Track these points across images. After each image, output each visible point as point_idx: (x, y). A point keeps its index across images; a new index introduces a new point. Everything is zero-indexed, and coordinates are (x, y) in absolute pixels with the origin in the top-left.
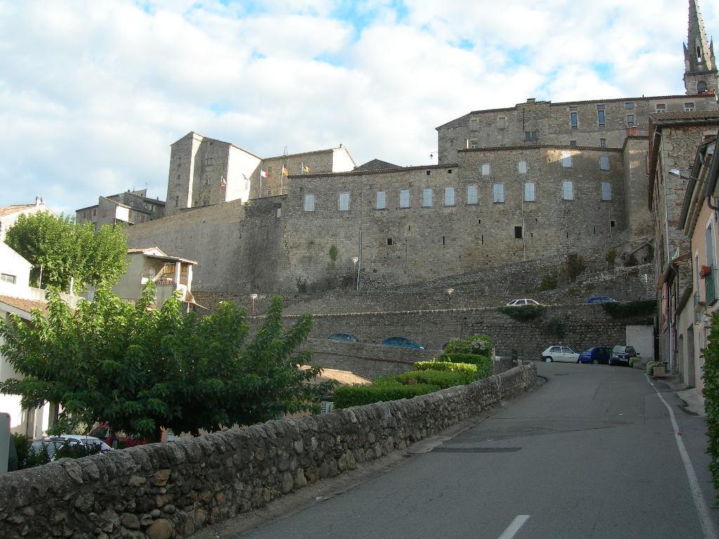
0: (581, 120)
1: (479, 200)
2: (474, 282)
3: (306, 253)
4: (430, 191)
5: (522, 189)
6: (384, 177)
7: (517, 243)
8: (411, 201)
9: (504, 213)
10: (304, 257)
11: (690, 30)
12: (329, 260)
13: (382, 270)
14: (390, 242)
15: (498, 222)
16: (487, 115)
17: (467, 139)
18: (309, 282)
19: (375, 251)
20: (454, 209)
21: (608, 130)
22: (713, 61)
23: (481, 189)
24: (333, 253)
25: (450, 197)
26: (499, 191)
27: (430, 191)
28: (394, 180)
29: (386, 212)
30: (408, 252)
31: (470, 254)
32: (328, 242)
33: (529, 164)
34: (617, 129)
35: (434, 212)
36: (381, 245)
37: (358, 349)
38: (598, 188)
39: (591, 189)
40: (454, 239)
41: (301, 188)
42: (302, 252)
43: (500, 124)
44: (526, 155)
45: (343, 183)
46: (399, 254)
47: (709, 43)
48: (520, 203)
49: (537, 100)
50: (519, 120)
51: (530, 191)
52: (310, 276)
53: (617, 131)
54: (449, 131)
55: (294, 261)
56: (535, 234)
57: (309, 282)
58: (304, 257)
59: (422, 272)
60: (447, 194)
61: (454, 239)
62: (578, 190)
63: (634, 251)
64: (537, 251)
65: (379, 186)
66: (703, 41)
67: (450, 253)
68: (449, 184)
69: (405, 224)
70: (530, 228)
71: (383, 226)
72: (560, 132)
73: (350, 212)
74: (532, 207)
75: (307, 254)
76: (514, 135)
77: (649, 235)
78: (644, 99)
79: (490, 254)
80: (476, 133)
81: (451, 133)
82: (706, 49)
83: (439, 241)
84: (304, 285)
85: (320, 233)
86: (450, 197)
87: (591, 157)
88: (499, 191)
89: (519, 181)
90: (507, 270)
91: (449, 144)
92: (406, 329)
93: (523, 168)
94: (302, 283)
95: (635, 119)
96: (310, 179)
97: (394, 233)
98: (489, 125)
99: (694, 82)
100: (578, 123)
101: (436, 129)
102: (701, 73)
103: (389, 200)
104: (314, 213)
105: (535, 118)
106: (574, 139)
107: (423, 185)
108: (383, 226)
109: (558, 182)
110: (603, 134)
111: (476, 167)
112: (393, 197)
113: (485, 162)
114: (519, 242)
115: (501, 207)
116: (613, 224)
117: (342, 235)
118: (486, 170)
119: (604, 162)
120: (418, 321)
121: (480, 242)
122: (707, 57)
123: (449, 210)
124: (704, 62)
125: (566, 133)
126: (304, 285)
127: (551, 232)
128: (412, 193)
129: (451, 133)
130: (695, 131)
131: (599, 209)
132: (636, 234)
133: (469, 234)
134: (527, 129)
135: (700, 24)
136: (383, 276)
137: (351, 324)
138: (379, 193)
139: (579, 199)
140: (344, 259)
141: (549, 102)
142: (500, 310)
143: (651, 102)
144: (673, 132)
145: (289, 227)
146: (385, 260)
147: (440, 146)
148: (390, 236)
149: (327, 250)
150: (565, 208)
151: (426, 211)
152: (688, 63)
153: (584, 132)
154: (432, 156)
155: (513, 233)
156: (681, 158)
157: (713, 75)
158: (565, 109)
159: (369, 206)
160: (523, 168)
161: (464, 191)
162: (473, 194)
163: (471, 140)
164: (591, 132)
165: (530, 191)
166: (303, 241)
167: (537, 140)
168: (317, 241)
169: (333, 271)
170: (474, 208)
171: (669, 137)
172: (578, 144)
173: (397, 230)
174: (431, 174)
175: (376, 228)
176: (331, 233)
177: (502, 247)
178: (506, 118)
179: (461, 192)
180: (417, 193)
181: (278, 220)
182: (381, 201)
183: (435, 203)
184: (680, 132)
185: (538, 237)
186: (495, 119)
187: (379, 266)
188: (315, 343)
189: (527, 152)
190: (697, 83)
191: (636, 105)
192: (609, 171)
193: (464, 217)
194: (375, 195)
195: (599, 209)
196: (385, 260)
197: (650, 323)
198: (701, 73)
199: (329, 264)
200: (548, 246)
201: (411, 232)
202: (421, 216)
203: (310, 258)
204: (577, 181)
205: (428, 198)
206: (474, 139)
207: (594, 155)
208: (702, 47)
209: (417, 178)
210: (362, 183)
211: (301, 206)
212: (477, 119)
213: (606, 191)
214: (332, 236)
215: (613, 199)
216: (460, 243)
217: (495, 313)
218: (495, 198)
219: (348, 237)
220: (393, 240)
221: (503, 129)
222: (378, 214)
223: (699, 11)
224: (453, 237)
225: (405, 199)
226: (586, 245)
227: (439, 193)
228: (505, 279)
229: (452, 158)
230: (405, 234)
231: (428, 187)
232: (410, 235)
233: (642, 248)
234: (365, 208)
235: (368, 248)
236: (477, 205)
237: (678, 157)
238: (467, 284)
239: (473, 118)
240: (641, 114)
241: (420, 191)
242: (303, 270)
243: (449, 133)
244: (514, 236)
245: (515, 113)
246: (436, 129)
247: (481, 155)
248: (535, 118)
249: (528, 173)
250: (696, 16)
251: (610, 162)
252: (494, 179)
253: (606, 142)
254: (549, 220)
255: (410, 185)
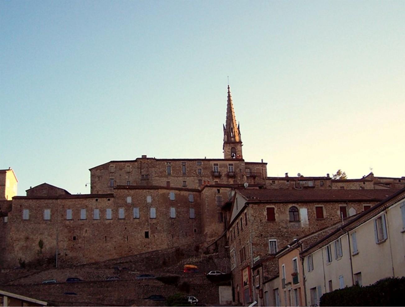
0: (173, 170)
1: (126, 216)
2: (126, 262)
3: (24, 244)
4: (98, 210)
5: (148, 211)
6: (71, 201)
7: (146, 240)
8: (87, 216)
9: (139, 224)
10: (23, 246)
11: (227, 118)
12: (38, 248)
13: (70, 255)
14: (74, 238)
15: (136, 229)
16: (120, 164)
17: (116, 180)
18: (27, 261)
19: (66, 244)
20: (111, 221)
21: (188, 177)
22: (240, 137)
23: (126, 210)
24: (41, 244)
25: (109, 214)
26: (136, 212)
27: (98, 210)
28: (77, 203)
29: (72, 222)
30: (85, 245)
31: (121, 246)
32: (37, 238)
33: (153, 198)
34: (192, 176)
35: (100, 222)
36: (69, 240)
37: (102, 300)
38: (188, 212)
39: (184, 212)
40: (111, 238)
41: (21, 206)
42: (22, 243)
43: (128, 169)
44: (151, 192)
45: (46, 204)
46: (80, 246)
47: (237, 126)
48: (148, 219)
49: (147, 157)
50: (138, 168)
51: (153, 212)
52: (27, 258)
53: (192, 177)
54: (98, 171)
55: (17, 249)
56: (155, 236)
57: (27, 261)
58: (23, 246)
59: (94, 256)
60: (107, 212)
61: (111, 238)
62: (178, 213)
63: (208, 246)
64: (157, 245)
65: (68, 206)
66: (235, 125)
67: (109, 245)
68: (109, 207)
69: (83, 229)
70: (153, 232)
71: (71, 229)
72: (162, 177)
73: (50, 220)
74: (154, 221)
75: (25, 245)
76: (134, 178)
77: (216, 238)
78: (205, 160)
79: (131, 246)
80: (114, 174)
81: (98, 173)
82: (236, 129)
83: (103, 239)
84: (24, 262)
85: (32, 232)
86: (109, 214)
87: (185, 195)
88: (136, 212)
89: (148, 207)
90: (143, 256)
91: (97, 179)
92: (109, 289)
93: (149, 199)
94: (23, 261)
95: (202, 171)
96: (26, 200)
97: (77, 233)
98: (121, 169)
99: (229, 148)
100: (171, 172)
101: (90, 170)
102: (233, 143)
103: (74, 215)
104: (28, 221)
105: (147, 167)
106: (169, 181)
107: (94, 207)
108: (71, 229)
109: (168, 208)
110: (184, 178)
111: (124, 198)
112: (77, 213)
113: (128, 195)
114: (147, 240)
115: (138, 220)
116: (195, 230)
117: (46, 233)
118: (129, 200)
119: (191, 197)
120: (115, 285)
121: (126, 240)
122: (236, 134)
123: (109, 221)
124: (234, 137)
125: (165, 177)
126: (24, 262)
127: (164, 235)
128: (87, 211)
129: (98, 173)
130: (262, 205)
131: (188, 222)
132: (209, 237)
133: (120, 235)
134: (143, 174)
135: (233, 115)
136: (71, 258)
137: (79, 287)
138: (68, 210)
139: (178, 217)
140: (47, 247)
141: (154, 159)
142: (158, 279)
143: (211, 162)
144: (254, 206)
145: (13, 229)
146: (72, 249)
147: (91, 180)
148: (75, 235)
149: (37, 243)
150: (172, 222)
151: (95, 222)
152: (226, 136)
153: (174, 177)
154: (86, 185)
155: (144, 235)
156: (257, 217)
157: (239, 144)
158: (164, 163)
159: (62, 217)
160: (149, 199)
161: (117, 211)
162: (122, 213)
163: (110, 177)
164: (178, 177)
165: (153, 212)
166: (22, 237)
167: (148, 180)
168: (31, 237)
169: (41, 255)
170: (123, 221)
171: (252, 207)
172: (172, 185)
173: (79, 232)
174: (98, 200)
175: (66, 230)
176: (39, 232)
177: (138, 242)
178: (131, 166)
179: (115, 212)
180: (90, 211)
181: (5, 224)
182: (69, 215)
183: (101, 217)
184: (256, 206)
185: (157, 237)
186: (124, 167)
187: (68, 252)
188: (78, 298)
189: (152, 191)
190: (231, 148)
191: (202, 163)
192: (193, 202)
193: (117, 225)
194: (65, 211)
195: (188, 222)
196: (72, 249)
197: (229, 284)
198: (233, 143)
199: (38, 251)
200: (162, 242)
201: (87, 233)
202: (93, 225)
203: (27, 247)
204: (177, 208)
205: (97, 214)
206: (112, 177)
207: (186, 194)
208: (234, 128)
209: (91, 203)
210: (58, 204)
211: (21, 216)
212: (114, 165)
213: (192, 211)
214: (41, 234)
215: (195, 218)
216: (115, 240)
217: (155, 280)
218: (134, 215)
219: (51, 236)
220: (77, 237)
221: (129, 172)
222: (67, 222)
223: (233, 106)
224: (111, 236)
225: (83, 214)
226: (183, 242)
227: (103, 211)
228: (143, 261)
229: (103, 189)
230: (84, 235)
231: (97, 208)
232: (86, 235)
233: (213, 244)
234: (60, 218)
235: (62, 242)
236: (124, 219)
237: (256, 216)
238: (123, 263)
239: (111, 165)
240: (205, 168)
241: (92, 210)
242: (23, 254)
243: (98, 173)
244: (144, 237)
245: (136, 163)
246: (90, 170)
247: (126, 191)
248: (147, 167)
249: (152, 202)
250: (231, 110)
251: (194, 197)
252: (133, 205)
253: (187, 183)
254: (163, 228)
255: (87, 207)
